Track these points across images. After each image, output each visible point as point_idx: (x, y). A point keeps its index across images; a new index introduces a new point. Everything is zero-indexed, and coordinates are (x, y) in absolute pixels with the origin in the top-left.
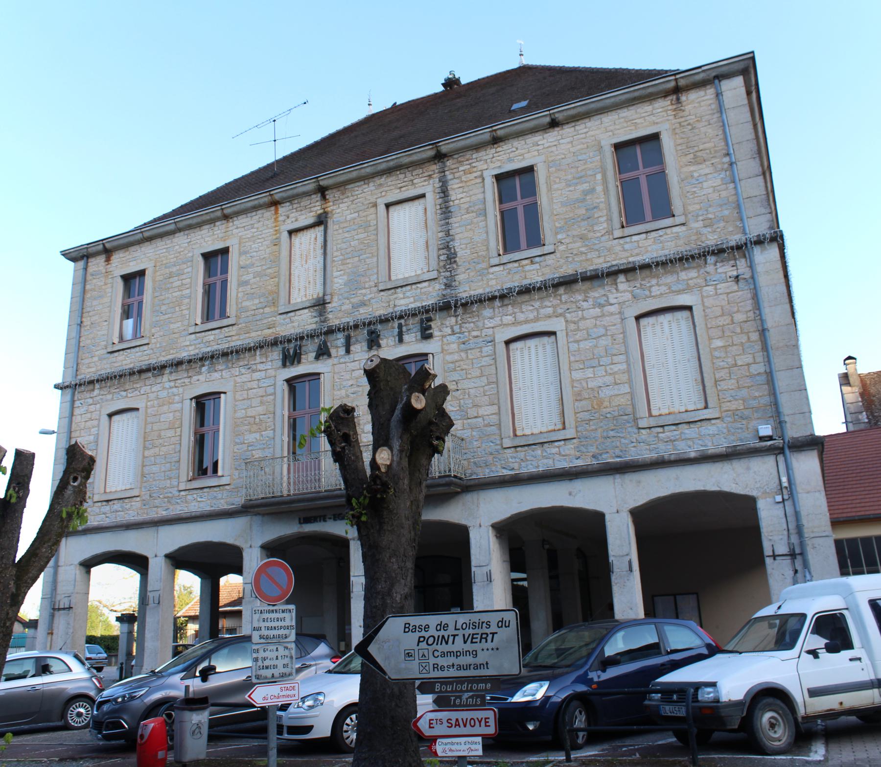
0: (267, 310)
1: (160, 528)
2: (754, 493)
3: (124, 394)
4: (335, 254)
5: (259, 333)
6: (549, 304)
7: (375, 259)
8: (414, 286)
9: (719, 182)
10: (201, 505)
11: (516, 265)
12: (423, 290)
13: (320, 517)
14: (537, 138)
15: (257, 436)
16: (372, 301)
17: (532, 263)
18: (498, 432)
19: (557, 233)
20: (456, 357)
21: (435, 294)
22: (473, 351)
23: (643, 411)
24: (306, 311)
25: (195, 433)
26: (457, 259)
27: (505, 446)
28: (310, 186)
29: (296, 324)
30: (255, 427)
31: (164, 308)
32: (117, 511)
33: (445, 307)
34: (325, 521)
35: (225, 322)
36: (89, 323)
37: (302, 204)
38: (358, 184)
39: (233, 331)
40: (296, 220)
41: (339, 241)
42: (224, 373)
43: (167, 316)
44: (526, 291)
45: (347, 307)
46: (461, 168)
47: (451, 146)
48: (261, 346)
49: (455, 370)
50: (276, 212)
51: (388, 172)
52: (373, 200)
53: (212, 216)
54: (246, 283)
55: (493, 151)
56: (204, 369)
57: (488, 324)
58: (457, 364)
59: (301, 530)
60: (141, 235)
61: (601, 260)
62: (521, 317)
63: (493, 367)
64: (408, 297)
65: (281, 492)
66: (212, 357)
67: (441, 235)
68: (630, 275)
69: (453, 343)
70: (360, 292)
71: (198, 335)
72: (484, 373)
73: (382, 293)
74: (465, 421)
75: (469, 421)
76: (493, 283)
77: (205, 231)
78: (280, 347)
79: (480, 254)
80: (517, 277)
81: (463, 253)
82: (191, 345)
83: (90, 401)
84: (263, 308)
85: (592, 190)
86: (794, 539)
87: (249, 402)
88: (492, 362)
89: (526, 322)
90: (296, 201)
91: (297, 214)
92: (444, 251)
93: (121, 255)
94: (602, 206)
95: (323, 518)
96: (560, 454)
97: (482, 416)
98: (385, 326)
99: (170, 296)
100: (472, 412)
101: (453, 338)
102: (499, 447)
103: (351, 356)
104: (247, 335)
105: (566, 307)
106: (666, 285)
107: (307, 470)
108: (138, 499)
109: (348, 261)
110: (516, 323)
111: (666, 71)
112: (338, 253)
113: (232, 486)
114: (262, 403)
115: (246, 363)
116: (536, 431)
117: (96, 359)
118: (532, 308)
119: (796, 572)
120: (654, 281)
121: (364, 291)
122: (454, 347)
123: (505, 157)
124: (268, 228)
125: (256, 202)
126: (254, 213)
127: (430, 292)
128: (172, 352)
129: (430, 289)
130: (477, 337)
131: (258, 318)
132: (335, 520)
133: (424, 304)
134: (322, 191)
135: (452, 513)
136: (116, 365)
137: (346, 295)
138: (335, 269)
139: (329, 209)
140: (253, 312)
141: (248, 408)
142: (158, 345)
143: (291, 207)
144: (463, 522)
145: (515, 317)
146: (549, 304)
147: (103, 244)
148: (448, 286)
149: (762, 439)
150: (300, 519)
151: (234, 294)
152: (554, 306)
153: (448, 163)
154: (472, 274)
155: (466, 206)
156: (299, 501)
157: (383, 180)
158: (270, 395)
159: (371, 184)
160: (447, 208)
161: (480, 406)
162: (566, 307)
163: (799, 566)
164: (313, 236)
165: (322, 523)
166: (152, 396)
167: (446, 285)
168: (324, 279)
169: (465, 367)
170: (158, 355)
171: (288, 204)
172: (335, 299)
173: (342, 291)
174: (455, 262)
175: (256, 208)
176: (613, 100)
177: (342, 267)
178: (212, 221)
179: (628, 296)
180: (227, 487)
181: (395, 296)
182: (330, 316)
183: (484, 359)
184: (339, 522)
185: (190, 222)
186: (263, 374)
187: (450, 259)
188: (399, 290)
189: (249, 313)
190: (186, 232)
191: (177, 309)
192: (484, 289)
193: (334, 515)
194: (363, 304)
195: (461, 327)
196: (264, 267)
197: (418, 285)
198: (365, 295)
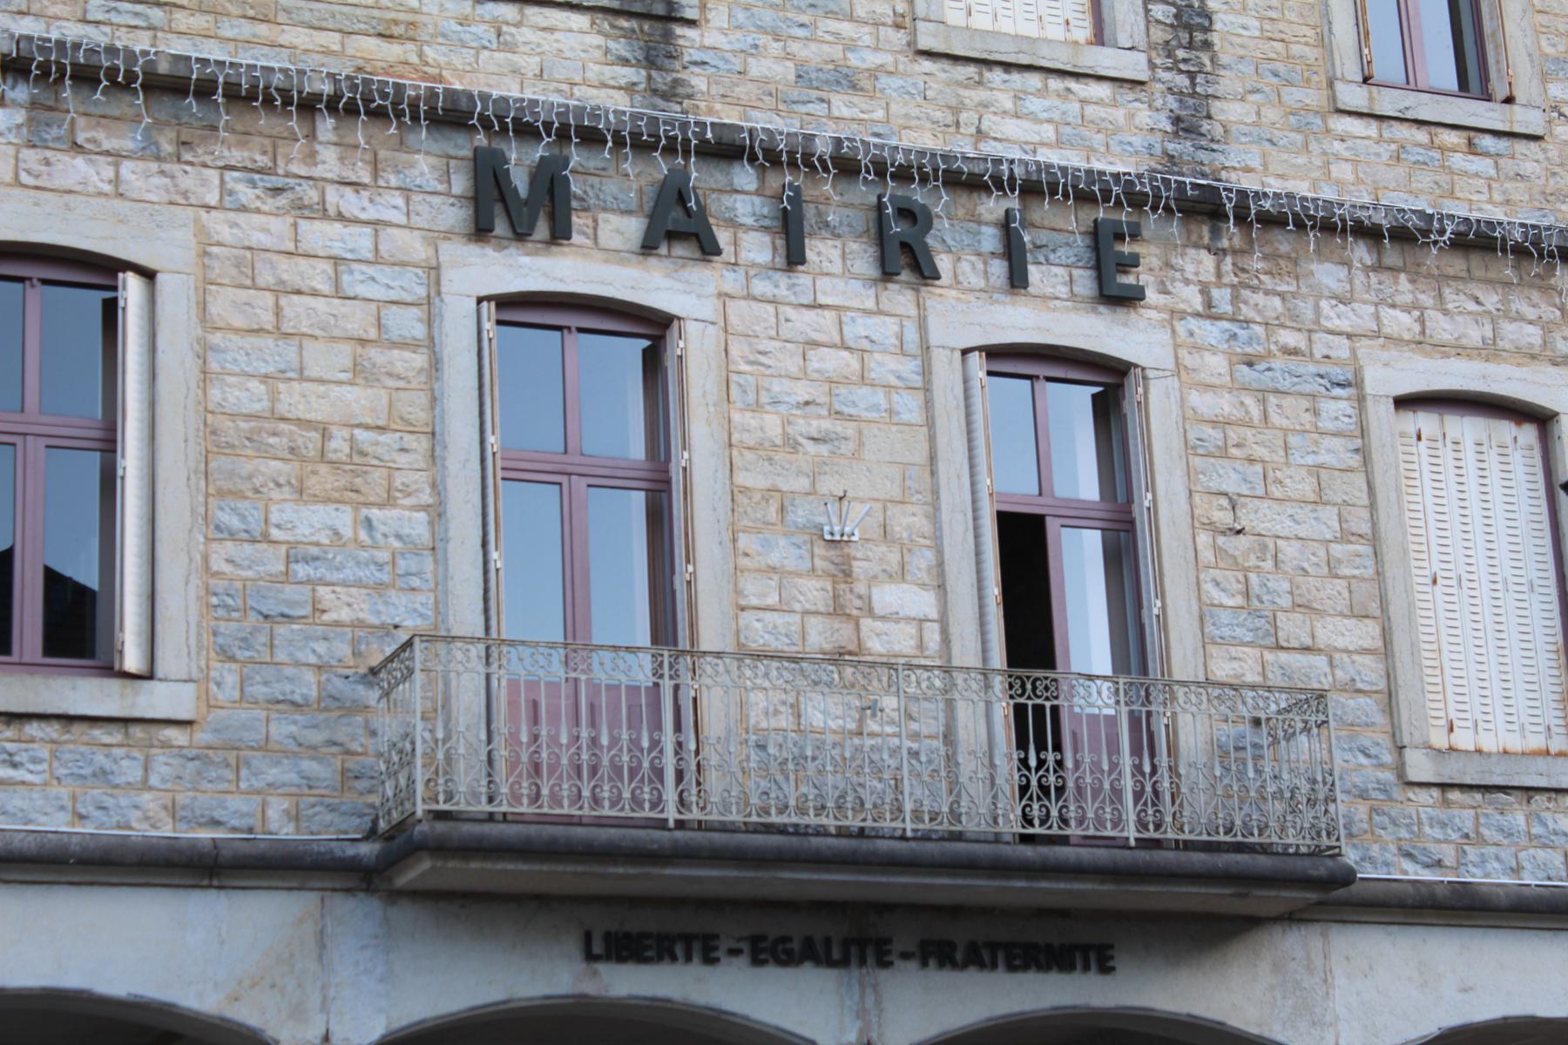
5: (332, 40)
6: (1531, 313)
8: (1055, 83)
11: (1421, 136)
12: (1090, 110)
13: (688, 939)
15: (344, 520)
17: (1472, 148)
18: (1380, 719)
20: (1224, 405)
21: (1138, 141)
22: (1287, 402)
25: (444, 467)
26: (1215, 38)
27: (1413, 775)
29: (530, 64)
33: (1205, 208)
34: (710, 960)
42: (127, 168)
44: (1477, 242)
49: (1223, 453)
57: (1336, 316)
58: (1233, 434)
59: (590, 988)
63: (1360, 480)
64: (1033, 118)
65: (955, 816)
69: (1212, 349)
70: (833, 25)
72: (1329, 495)
73: (927, 65)
74: (1268, 656)
75: (1283, 657)
76: (1343, 171)
78: (661, 167)
79: (1296, 49)
80: (1424, 180)
88: (1355, 461)
89: (1459, 350)
97: (1329, 653)
100: (1293, 627)
101: (1211, 332)
102: (1388, 776)
103: (802, 279)
104: (263, 30)
110: (1422, 342)
113: (202, 736)
114: (360, 373)
115: (263, 160)
116: (1489, 743)
118: (1472, 306)
121: (846, 28)
122: (1216, 364)
127: (1118, 130)
129: (1119, 115)
130: (1294, 352)
132: (757, 961)
133: (1097, 166)
141: (282, 375)
145: (1421, 321)
146: (1531, 313)
148: (1183, 127)
150: (588, 938)
152: (1547, 328)
154: (1271, 114)
156: (715, 856)
158: (403, 345)
161: (1321, 613)
165: (696, 969)
167: (1177, 120)
169: (1260, 452)
174: (1207, 45)
180: (170, 733)
181: (980, 94)
183: (1328, 442)
184: (772, 973)
186: (361, 240)
187: (1190, 28)
188: (997, 76)
192: (1314, 186)
194: (848, 81)
195: (1235, 299)
197: (1072, 84)
198: (851, 46)
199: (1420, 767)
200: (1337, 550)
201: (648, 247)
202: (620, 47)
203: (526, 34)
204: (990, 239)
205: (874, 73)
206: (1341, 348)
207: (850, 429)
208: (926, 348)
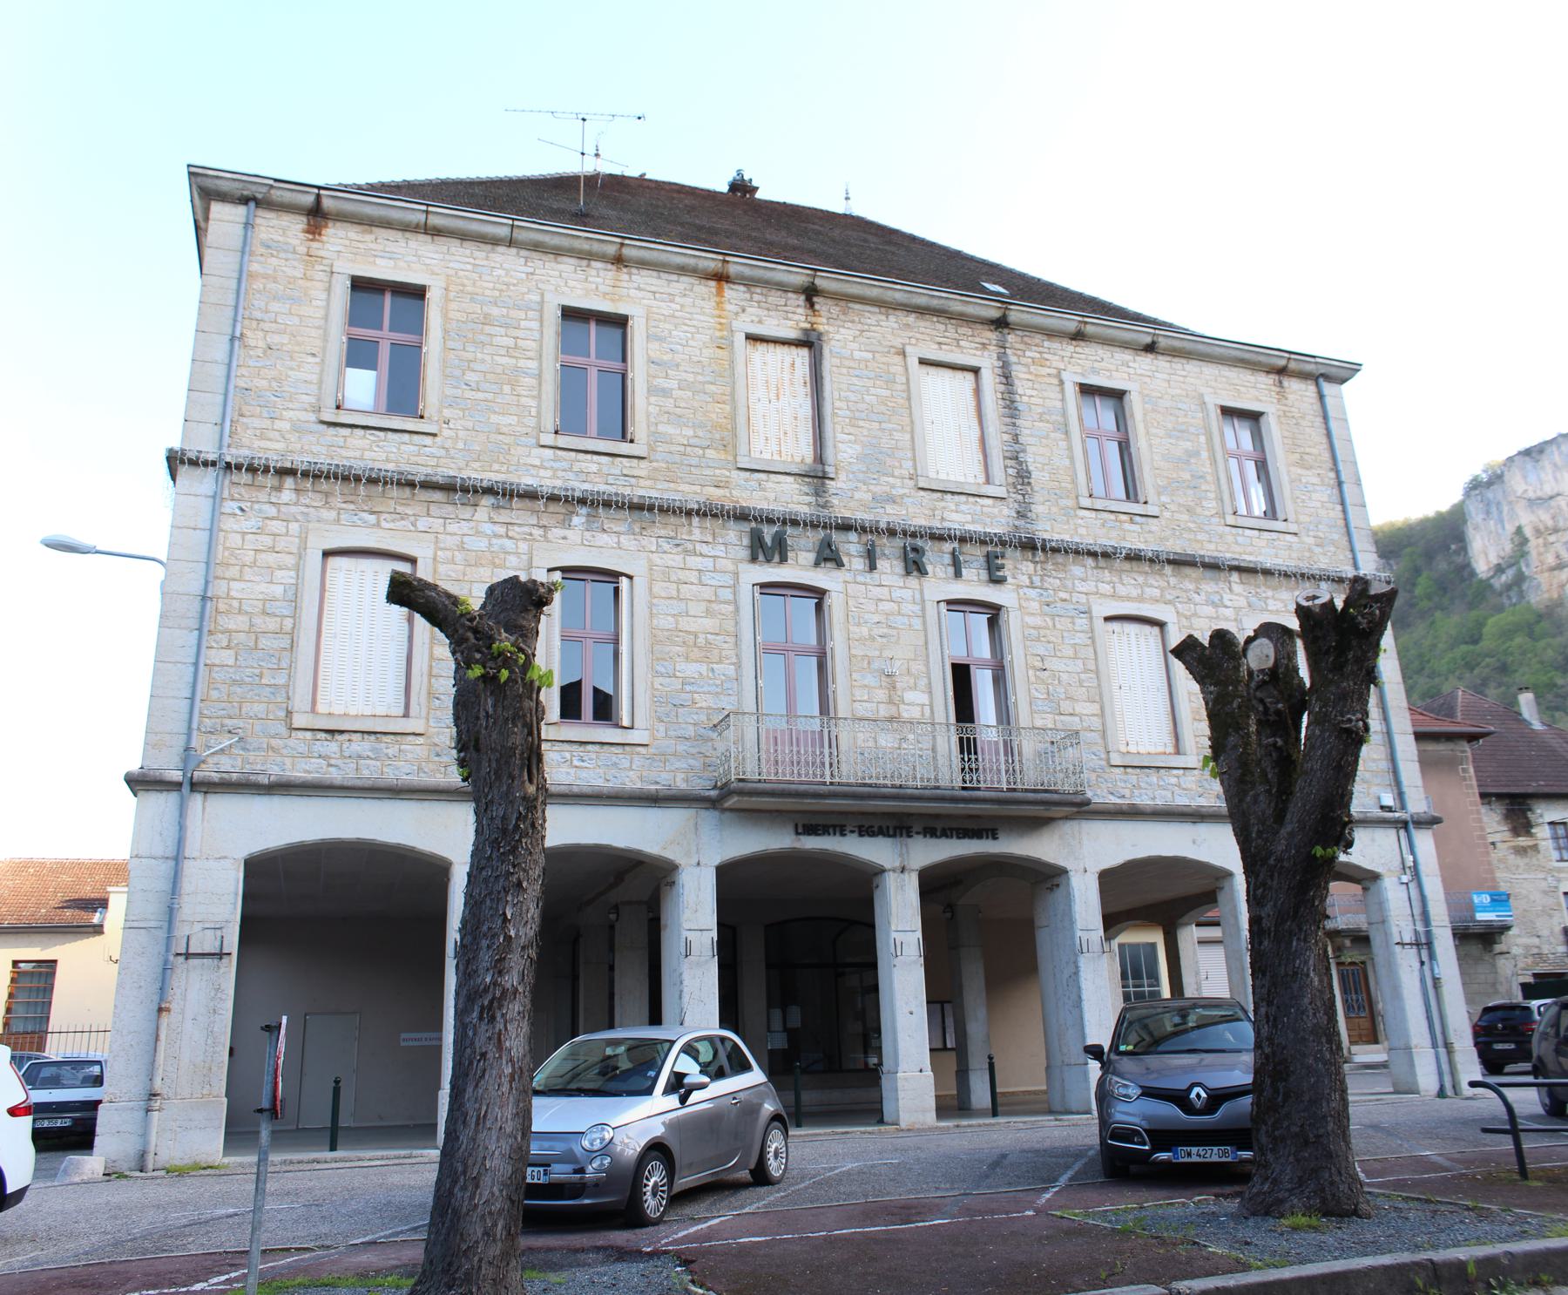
0: (710, 453)
1: (211, 797)
4: (838, 404)
5: (698, 489)
7: (908, 437)
8: (971, 499)
9: (1325, 499)
10: (584, 774)
11: (1112, 517)
13: (834, 827)
15: (703, 669)
17: (1132, 521)
19: (1159, 494)
20: (1038, 621)
23: (300, 701)
24: (791, 479)
30: (696, 653)
31: (471, 377)
32: (360, 757)
33: (1029, 546)
34: (843, 835)
35: (624, 448)
36: (261, 344)
37: (770, 299)
39: (641, 468)
40: (760, 322)
41: (844, 386)
42: (622, 538)
43: (480, 395)
45: (863, 495)
48: (708, 512)
50: (720, 293)
51: (922, 311)
52: (898, 342)
53: (596, 247)
54: (665, 393)
55: (1071, 348)
56: (576, 520)
58: (1042, 632)
59: (797, 845)
61: (1212, 547)
62: (1121, 590)
63: (1091, 649)
64: (962, 512)
66: (313, 475)
68: (1244, 576)
71: (560, 453)
76: (1082, 531)
77: (568, 265)
78: (821, 533)
80: (1114, 534)
82: (542, 467)
83: (272, 511)
84: (703, 448)
85: (1197, 454)
86: (1420, 928)
87: (683, 605)
89: (1129, 598)
90: (758, 290)
92: (1012, 463)
94: (1209, 478)
95: (841, 830)
96: (1179, 786)
97: (1080, 716)
98: (937, 544)
100: (1066, 706)
101: (1032, 593)
103: (875, 575)
107: (822, 746)
108: (421, 740)
109: (861, 423)
111: (1170, 325)
114: (709, 613)
119: (1422, 963)
120: (1270, 593)
121: (891, 480)
122: (1035, 606)
123: (1088, 364)
124: (704, 314)
125: (692, 261)
126: (675, 277)
128: (496, 467)
131: (694, 461)
132: (861, 835)
134: (810, 294)
135: (1042, 847)
136: (344, 453)
139: (821, 328)
143: (748, 296)
144: (1061, 863)
147: (318, 196)
148: (1021, 515)
149: (1382, 807)
154: (1054, 509)
156: (845, 796)
157: (911, 318)
159: (892, 318)
163: (1425, 958)
164: (788, 360)
165: (838, 838)
166: (451, 541)
170: (462, 464)
171: (742, 288)
172: (842, 476)
173: (855, 468)
175: (683, 270)
176: (1222, 350)
177: (852, 430)
178: (588, 256)
179: (1242, 602)
181: (943, 504)
182: (835, 501)
186: (709, 563)
190: (524, 253)
194: (892, 500)
196: (700, 378)
198: (893, 487)
201: (817, 564)
202: (805, 489)
203: (770, 485)
204: (947, 559)
205: (902, 496)
206: (1083, 599)
207: (894, 632)
208: (923, 601)
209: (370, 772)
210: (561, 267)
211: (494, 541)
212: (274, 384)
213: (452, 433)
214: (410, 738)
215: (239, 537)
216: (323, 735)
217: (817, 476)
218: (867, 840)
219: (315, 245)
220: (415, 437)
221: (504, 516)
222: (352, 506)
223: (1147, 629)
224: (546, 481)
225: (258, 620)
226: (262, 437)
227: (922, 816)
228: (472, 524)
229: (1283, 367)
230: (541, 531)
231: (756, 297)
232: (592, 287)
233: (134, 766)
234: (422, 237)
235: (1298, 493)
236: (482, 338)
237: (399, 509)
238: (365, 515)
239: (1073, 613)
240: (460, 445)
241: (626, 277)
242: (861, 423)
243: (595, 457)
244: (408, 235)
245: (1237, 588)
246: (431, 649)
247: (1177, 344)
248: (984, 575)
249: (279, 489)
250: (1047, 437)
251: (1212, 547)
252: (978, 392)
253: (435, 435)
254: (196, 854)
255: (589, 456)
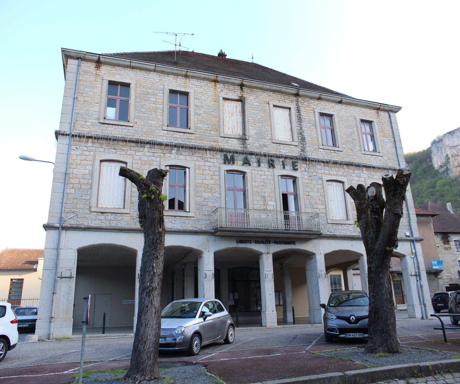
2: (405, 254)
3: (114, 151)
4: (249, 118)
5: (209, 143)
7: (270, 128)
8: (288, 146)
10: (175, 225)
11: (329, 151)
13: (248, 241)
14: (333, 104)
15: (210, 195)
16: (269, 146)
17: (334, 152)
20: (307, 181)
23: (93, 204)
24: (235, 140)
28: (238, 81)
30: (208, 190)
32: (111, 220)
33: (305, 159)
34: (250, 243)
35: (187, 131)
36: (82, 100)
38: (258, 90)
39: (193, 137)
40: (227, 94)
41: (251, 113)
43: (146, 115)
44: (335, 163)
46: (305, 104)
47: (304, 93)
48: (212, 149)
50: (215, 86)
51: (274, 91)
52: (267, 100)
53: (179, 72)
54: (200, 115)
55: (317, 102)
56: (173, 152)
57: (320, 171)
59: (237, 246)
60: (129, 63)
61: (358, 160)
66: (97, 138)
67: (298, 128)
73: (274, 144)
76: (320, 155)
77: (171, 77)
78: (244, 156)
80: (329, 156)
81: (308, 139)
83: (85, 149)
85: (354, 133)
88: (322, 187)
89: (334, 175)
90: (227, 85)
91: (228, 91)
93: (109, 68)
94: (357, 140)
97: (319, 209)
99: (148, 104)
100: (315, 206)
101: (306, 173)
103: (260, 168)
105: (347, 173)
106: (378, 176)
107: (244, 217)
108: (128, 215)
109: (256, 124)
112: (251, 118)
113: (195, 218)
114: (212, 179)
117: (89, 124)
119: (417, 281)
120: (374, 174)
121: (265, 140)
122: (306, 177)
123: (322, 107)
124: (211, 92)
125: (207, 76)
126: (202, 81)
128: (150, 136)
129: (295, 149)
131: (208, 135)
132: (256, 243)
134: (242, 86)
136: (106, 132)
137: (256, 139)
138: (250, 125)
139: (245, 96)
140: (204, 131)
142: (140, 130)
143: (223, 87)
144: (314, 251)
147: (99, 57)
148: (302, 150)
151: (379, 140)
152: (343, 172)
153: (299, 99)
154: (312, 149)
155: (308, 120)
156: (251, 232)
157: (271, 93)
160: (300, 118)
162: (347, 173)
163: (418, 279)
164: (235, 105)
165: (249, 244)
166: (137, 158)
168: (292, 133)
170: (141, 135)
171: (222, 84)
172: (251, 139)
175: (205, 79)
177: (254, 126)
178: (177, 75)
179: (366, 176)
180: (192, 218)
182: (248, 146)
185: (165, 70)
186: (212, 164)
189: (202, 131)
190: (158, 74)
191: (153, 113)
193: (256, 241)
194: (265, 146)
196: (210, 110)
198: (265, 142)
199: (329, 222)
200: (320, 197)
201: (243, 165)
202: (240, 143)
203: (230, 141)
204: (281, 163)
205: (268, 145)
206: (320, 175)
209: (114, 224)
210: (170, 78)
211: (150, 157)
212: (86, 112)
213: (137, 126)
214: (125, 215)
215: (76, 156)
216: (100, 214)
217: (243, 139)
218: (257, 244)
219: (98, 71)
220: (127, 127)
221: (153, 150)
222: (108, 147)
223: (339, 184)
224: (165, 140)
225: (81, 180)
226: (82, 127)
227: (273, 237)
228: (143, 153)
229: (379, 108)
230: (163, 155)
231: (226, 87)
232: (178, 84)
233: (46, 222)
234: (129, 69)
235: (383, 144)
236: (146, 98)
237: (122, 148)
238: (112, 150)
239: (317, 179)
240: (140, 130)
241: (188, 81)
242: (256, 124)
243: (179, 133)
244: (125, 68)
245: (365, 172)
246: (131, 189)
247: (348, 101)
248: (292, 168)
249: (87, 142)
250: (310, 128)
251: (358, 160)
252: (290, 115)
253: (132, 127)
254: (63, 248)
255: (177, 133)
